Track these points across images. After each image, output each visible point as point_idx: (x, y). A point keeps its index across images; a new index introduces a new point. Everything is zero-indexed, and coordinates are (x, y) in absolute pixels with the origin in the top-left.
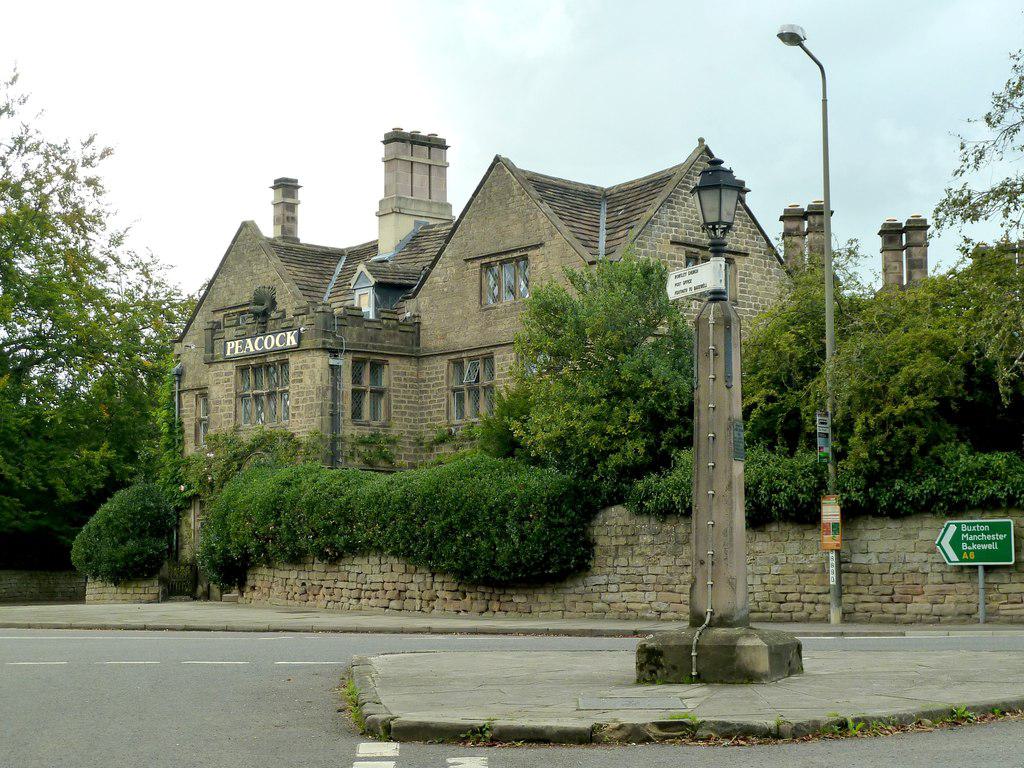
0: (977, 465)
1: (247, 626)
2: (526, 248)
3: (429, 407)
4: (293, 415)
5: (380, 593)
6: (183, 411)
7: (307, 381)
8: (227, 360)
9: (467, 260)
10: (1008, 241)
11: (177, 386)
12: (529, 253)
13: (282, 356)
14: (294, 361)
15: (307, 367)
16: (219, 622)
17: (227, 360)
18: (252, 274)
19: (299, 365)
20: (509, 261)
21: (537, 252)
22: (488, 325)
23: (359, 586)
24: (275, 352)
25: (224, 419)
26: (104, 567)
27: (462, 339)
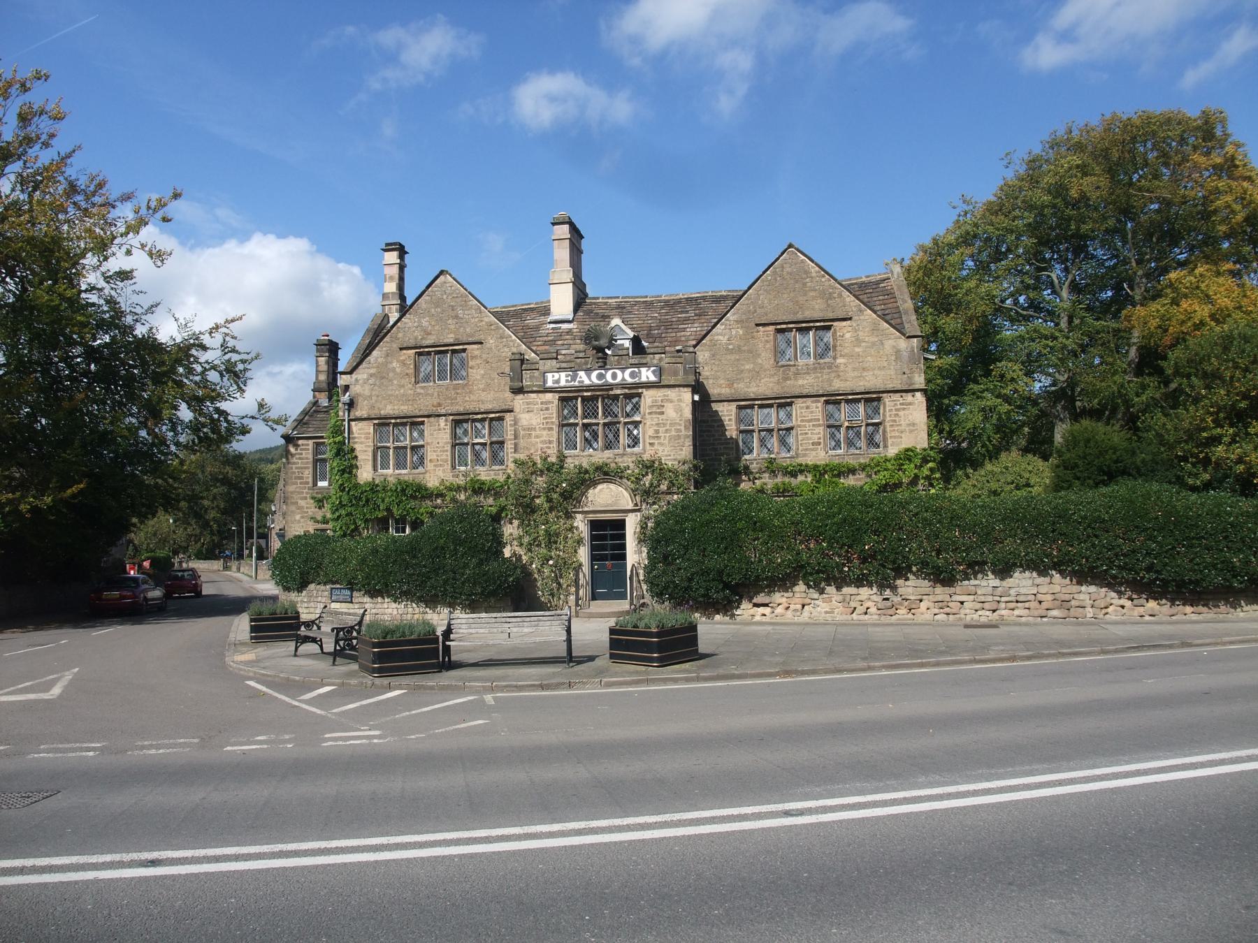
0: (1130, 483)
3: (714, 444)
5: (1033, 605)
6: (354, 438)
8: (550, 390)
9: (757, 325)
10: (236, 374)
11: (346, 414)
12: (835, 324)
13: (633, 393)
14: (649, 396)
17: (550, 390)
18: (457, 317)
19: (660, 399)
21: (844, 323)
22: (786, 379)
23: (998, 598)
24: (623, 385)
27: (754, 389)
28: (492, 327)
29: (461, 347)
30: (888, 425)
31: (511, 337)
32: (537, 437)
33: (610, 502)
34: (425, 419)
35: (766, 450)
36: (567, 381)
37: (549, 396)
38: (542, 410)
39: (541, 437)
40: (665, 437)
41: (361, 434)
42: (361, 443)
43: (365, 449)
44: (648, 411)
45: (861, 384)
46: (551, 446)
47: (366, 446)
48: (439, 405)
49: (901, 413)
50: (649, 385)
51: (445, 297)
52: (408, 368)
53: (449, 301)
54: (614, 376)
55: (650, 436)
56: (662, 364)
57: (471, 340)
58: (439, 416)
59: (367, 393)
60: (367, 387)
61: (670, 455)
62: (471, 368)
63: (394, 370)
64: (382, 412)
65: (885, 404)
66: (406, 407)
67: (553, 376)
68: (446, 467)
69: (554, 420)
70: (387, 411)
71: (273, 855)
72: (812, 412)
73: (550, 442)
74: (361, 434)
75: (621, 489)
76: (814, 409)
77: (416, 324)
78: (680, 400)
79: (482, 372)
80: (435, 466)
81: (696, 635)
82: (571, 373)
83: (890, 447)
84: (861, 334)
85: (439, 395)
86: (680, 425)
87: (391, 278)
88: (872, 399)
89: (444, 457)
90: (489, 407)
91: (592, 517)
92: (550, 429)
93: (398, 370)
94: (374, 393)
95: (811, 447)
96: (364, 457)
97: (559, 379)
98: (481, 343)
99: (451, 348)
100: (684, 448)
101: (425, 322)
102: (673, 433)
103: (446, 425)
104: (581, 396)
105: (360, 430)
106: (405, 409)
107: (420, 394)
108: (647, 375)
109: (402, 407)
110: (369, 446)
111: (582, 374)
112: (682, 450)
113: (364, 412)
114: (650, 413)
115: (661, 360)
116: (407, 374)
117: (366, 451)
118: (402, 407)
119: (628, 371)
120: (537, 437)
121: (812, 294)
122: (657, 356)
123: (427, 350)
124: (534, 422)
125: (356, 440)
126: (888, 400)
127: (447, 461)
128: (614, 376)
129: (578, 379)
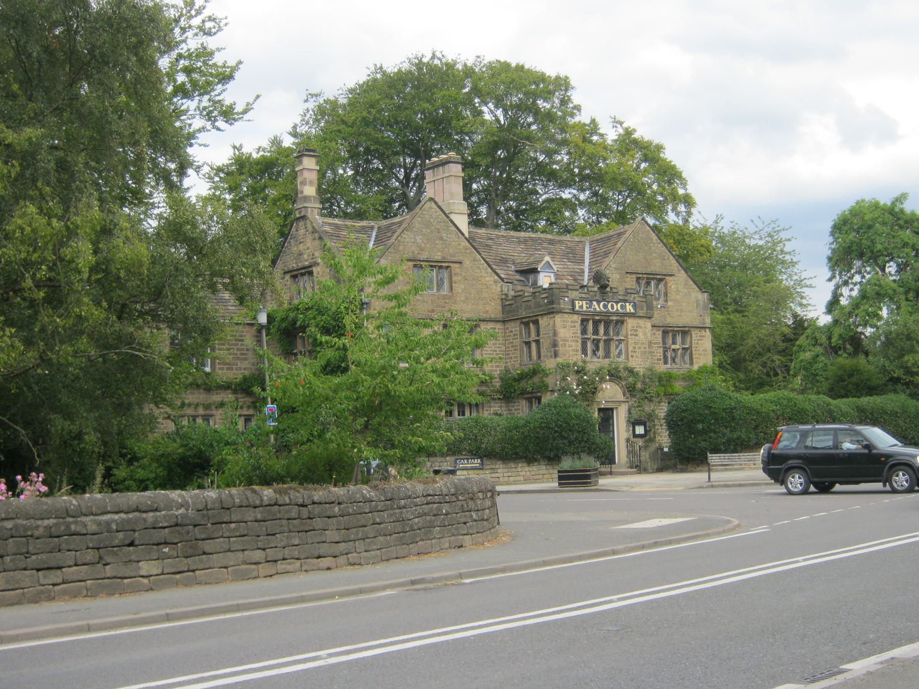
1: (843, 496)
2: (665, 275)
4: (632, 356)
7: (641, 335)
8: (577, 313)
9: (627, 273)
14: (631, 323)
15: (640, 327)
17: (577, 313)
18: (441, 239)
20: (435, 266)
24: (616, 313)
25: (571, 353)
28: (468, 251)
29: (447, 264)
30: (693, 349)
32: (570, 346)
48: (433, 311)
49: (700, 342)
51: (432, 220)
53: (435, 224)
54: (612, 307)
56: (636, 301)
57: (453, 259)
65: (691, 335)
71: (867, 547)
73: (577, 351)
77: (412, 240)
78: (645, 327)
87: (311, 183)
88: (685, 332)
92: (577, 341)
98: (461, 263)
101: (419, 239)
102: (643, 350)
107: (419, 300)
108: (629, 308)
111: (595, 303)
115: (634, 298)
119: (619, 304)
120: (570, 346)
121: (654, 255)
122: (633, 296)
124: (568, 335)
126: (695, 334)
128: (612, 307)
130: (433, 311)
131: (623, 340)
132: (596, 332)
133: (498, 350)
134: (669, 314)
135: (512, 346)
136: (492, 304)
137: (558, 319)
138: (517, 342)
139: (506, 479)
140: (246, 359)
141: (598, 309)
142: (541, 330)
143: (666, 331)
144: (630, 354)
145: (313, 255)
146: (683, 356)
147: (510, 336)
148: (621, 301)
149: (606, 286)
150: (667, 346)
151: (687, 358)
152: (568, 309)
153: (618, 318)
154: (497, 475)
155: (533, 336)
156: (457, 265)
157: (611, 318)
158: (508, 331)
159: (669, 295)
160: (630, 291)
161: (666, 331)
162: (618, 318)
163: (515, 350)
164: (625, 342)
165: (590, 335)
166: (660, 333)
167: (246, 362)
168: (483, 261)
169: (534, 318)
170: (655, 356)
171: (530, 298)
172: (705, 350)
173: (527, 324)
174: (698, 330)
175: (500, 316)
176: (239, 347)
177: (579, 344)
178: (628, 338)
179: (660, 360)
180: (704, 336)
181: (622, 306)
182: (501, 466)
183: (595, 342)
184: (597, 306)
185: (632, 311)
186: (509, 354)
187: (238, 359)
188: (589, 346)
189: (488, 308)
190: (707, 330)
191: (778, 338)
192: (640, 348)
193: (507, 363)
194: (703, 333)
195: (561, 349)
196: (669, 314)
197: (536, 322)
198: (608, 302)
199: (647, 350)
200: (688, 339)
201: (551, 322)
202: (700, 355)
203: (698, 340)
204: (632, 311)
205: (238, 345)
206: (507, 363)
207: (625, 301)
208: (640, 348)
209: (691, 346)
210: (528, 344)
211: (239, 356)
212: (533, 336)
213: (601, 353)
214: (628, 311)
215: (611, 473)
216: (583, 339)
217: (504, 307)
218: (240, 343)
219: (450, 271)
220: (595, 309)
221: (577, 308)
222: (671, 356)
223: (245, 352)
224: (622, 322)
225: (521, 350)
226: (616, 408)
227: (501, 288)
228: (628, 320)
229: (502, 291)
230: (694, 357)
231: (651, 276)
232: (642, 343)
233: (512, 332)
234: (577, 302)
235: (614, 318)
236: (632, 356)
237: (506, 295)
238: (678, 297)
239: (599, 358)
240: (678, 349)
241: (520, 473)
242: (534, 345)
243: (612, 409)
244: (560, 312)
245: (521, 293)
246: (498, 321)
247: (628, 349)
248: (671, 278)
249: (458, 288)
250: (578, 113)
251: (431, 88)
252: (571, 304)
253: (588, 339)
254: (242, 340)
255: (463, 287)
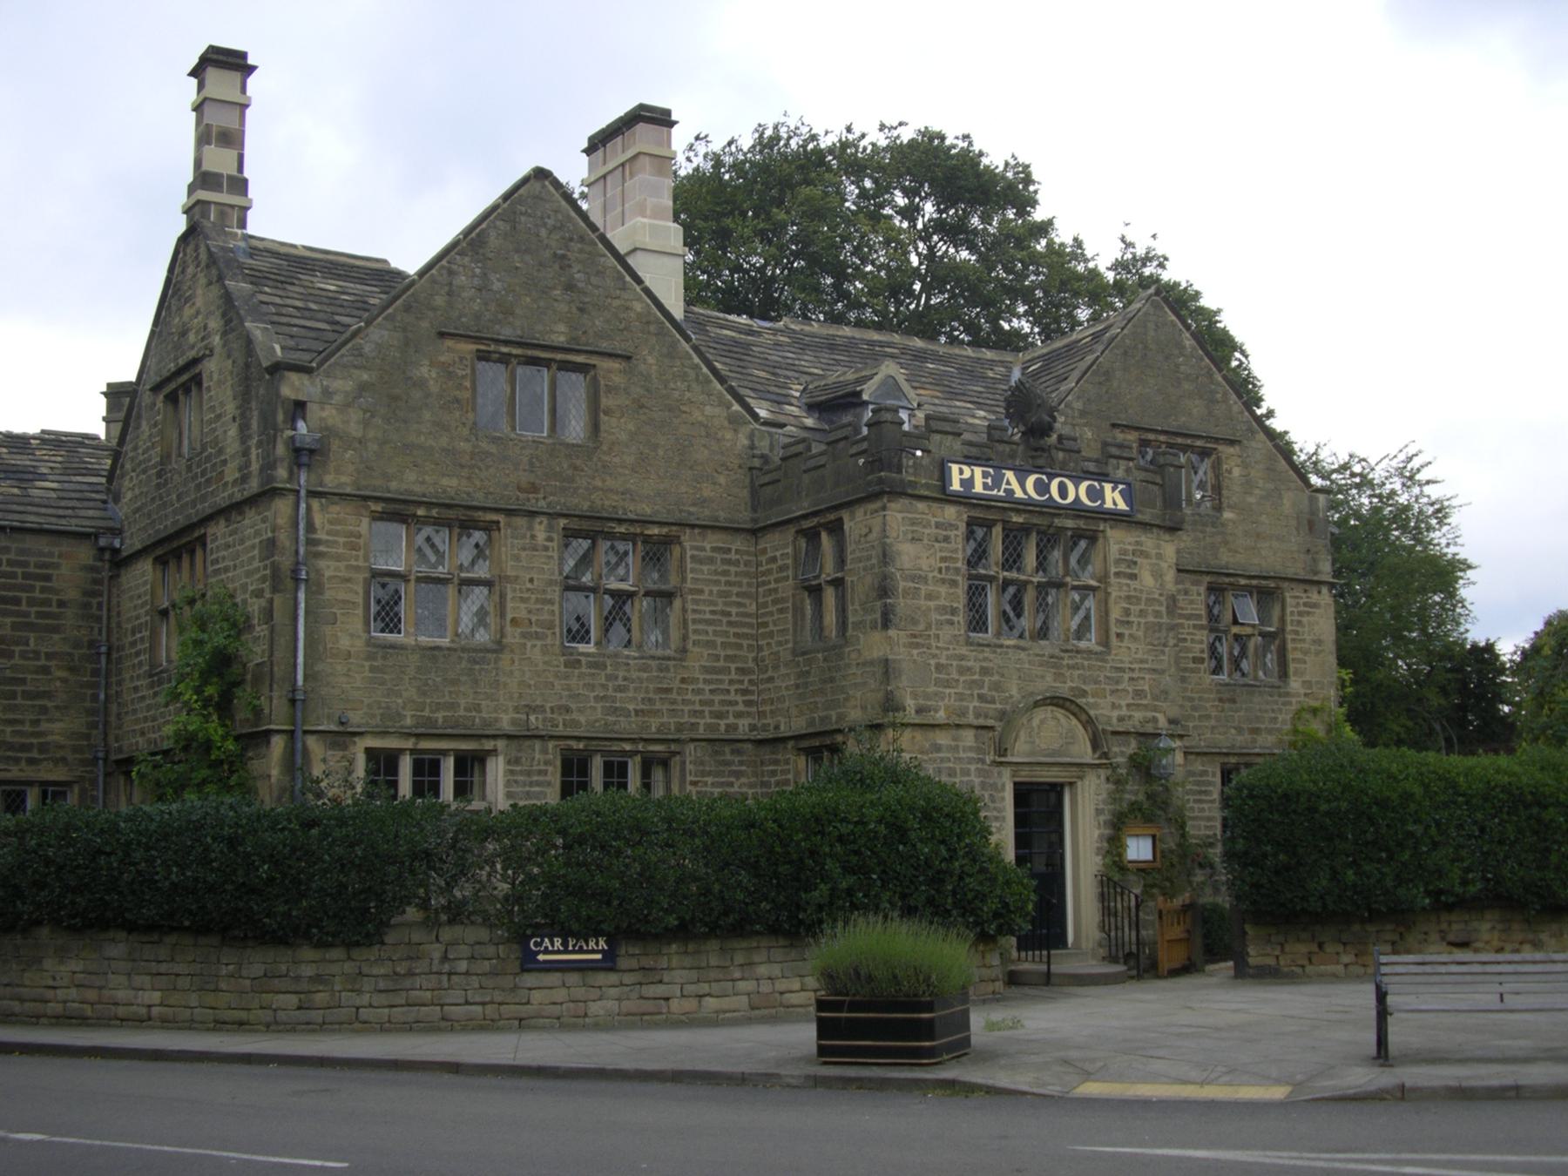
2: (1217, 440)
7: (1147, 580)
9: (1114, 426)
12: (1220, 448)
14: (1117, 541)
16: (1349, 1088)
18: (570, 287)
19: (1130, 548)
24: (1076, 509)
25: (935, 616)
26: (444, 917)
30: (1289, 637)
31: (690, 358)
33: (1056, 746)
34: (501, 518)
35: (1239, 673)
36: (985, 486)
37: (950, 512)
38: (937, 540)
39: (938, 598)
40: (1139, 623)
41: (336, 533)
42: (338, 558)
43: (347, 575)
44: (1113, 570)
45: (1256, 561)
46: (955, 619)
47: (348, 567)
48: (534, 488)
49: (1305, 620)
50: (1115, 517)
51: (543, 233)
52: (460, 387)
54: (1063, 491)
55: (1117, 620)
57: (604, 345)
58: (532, 514)
59: (355, 430)
60: (355, 415)
61: (1146, 661)
62: (606, 413)
63: (421, 384)
64: (394, 485)
66: (454, 482)
67: (961, 472)
68: (549, 641)
69: (959, 565)
70: (404, 487)
72: (1192, 602)
73: (954, 611)
74: (336, 533)
75: (1074, 721)
76: (1195, 597)
77: (476, 282)
78: (1159, 556)
79: (631, 427)
80: (524, 635)
81: (969, 1036)
82: (991, 470)
83: (1292, 678)
84: (1253, 473)
85: (531, 464)
86: (1161, 604)
88: (1267, 592)
89: (546, 617)
90: (646, 509)
91: (1025, 776)
92: (954, 583)
93: (434, 388)
94: (371, 434)
95: (1192, 665)
96: (341, 596)
97: (972, 476)
98: (628, 358)
99: (560, 356)
100: (1167, 649)
102: (1151, 619)
103: (550, 539)
104: (1004, 522)
105: (331, 522)
106: (451, 485)
107: (489, 454)
108: (1113, 498)
109: (445, 482)
110: (357, 569)
111: (1010, 475)
112: (1163, 652)
113: (344, 479)
114: (1117, 574)
116: (457, 401)
117: (348, 580)
118: (445, 482)
120: (929, 597)
123: (505, 350)
124: (925, 566)
125: (322, 548)
126: (1293, 598)
127: (551, 626)
128: (1063, 491)
129: (1004, 486)
130: (534, 488)
131: (1093, 589)
132: (1012, 560)
133: (734, 610)
134: (1226, 543)
135: (775, 602)
136: (722, 480)
137: (896, 515)
138: (787, 588)
139: (689, 1005)
140: (56, 629)
141: (1019, 494)
142: (849, 549)
143: (1220, 586)
144: (1114, 629)
145: (205, 327)
146: (1262, 652)
147: (769, 572)
148: (1087, 475)
149: (1045, 430)
150: (1222, 626)
151: (1270, 659)
152: (927, 486)
153: (1081, 524)
154: (660, 990)
155: (829, 570)
156: (615, 365)
157: (1057, 522)
158: (763, 559)
159: (1225, 492)
160: (1114, 451)
161: (1220, 586)
162: (1081, 524)
163: (781, 611)
164: (1100, 595)
165: (993, 566)
166: (1202, 589)
167: (56, 637)
168: (697, 360)
169: (832, 517)
170: (1188, 650)
171: (823, 460)
172: (1318, 642)
173: (812, 536)
174: (1302, 586)
175: (744, 517)
176: (37, 594)
177: (961, 592)
178: (1107, 584)
179: (1202, 660)
180: (1315, 606)
181: (1090, 490)
182: (675, 962)
183: (1011, 590)
184: (1015, 486)
185: (1122, 506)
186: (765, 624)
187: (31, 627)
188: (992, 602)
189: (707, 491)
190: (1325, 590)
191: (1468, 626)
192: (1142, 613)
193: (760, 648)
194: (1315, 597)
195: (901, 604)
196: (1226, 543)
197: (836, 529)
198: (1051, 477)
199: (1165, 620)
200: (1276, 613)
201: (876, 523)
202: (1306, 652)
203: (1300, 614)
204: (1122, 506)
205: (31, 589)
206: (760, 648)
207: (1103, 477)
208: (1142, 613)
209: (1282, 630)
210: (815, 591)
211: (33, 619)
212: (829, 570)
213: (1026, 622)
214: (1109, 505)
215: (1047, 979)
216: (970, 577)
217: (754, 491)
218: (38, 584)
219: (595, 380)
220: (1011, 492)
221: (956, 486)
222: (1231, 653)
223: (55, 609)
224: (1093, 538)
225: (798, 611)
226: (1071, 784)
227: (751, 436)
228: (1109, 532)
229: (752, 447)
230: (1290, 656)
231: (1179, 440)
232: (1150, 601)
233: (774, 559)
234: (955, 468)
235: (1070, 523)
236: (1119, 636)
237: (763, 456)
238: (1251, 500)
239: (1021, 636)
240: (1249, 636)
241: (742, 985)
242: (829, 595)
243: (1056, 789)
244: (899, 492)
245: (800, 448)
246: (737, 530)
247: (1107, 613)
248: (1231, 450)
249: (617, 428)
250: (1037, 186)
251: (787, 184)
252: (937, 474)
253: (991, 579)
254: (48, 578)
255: (631, 427)
